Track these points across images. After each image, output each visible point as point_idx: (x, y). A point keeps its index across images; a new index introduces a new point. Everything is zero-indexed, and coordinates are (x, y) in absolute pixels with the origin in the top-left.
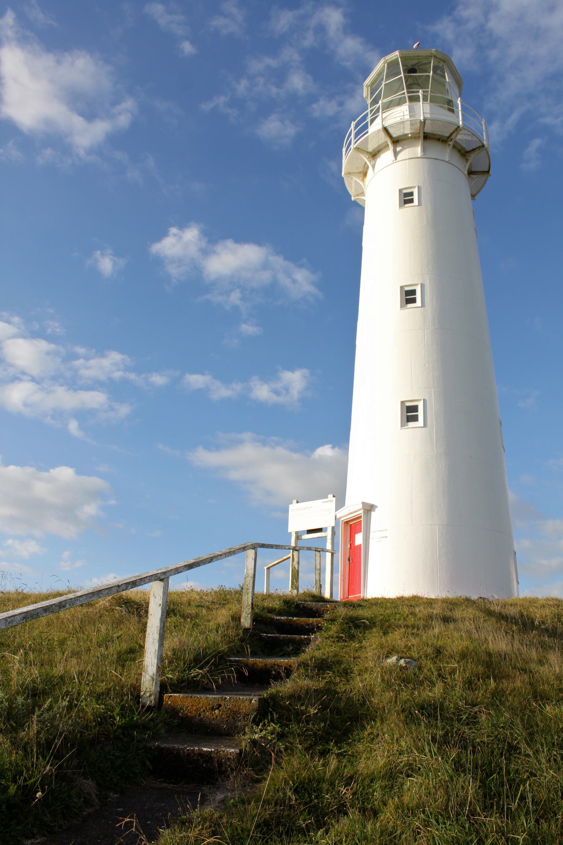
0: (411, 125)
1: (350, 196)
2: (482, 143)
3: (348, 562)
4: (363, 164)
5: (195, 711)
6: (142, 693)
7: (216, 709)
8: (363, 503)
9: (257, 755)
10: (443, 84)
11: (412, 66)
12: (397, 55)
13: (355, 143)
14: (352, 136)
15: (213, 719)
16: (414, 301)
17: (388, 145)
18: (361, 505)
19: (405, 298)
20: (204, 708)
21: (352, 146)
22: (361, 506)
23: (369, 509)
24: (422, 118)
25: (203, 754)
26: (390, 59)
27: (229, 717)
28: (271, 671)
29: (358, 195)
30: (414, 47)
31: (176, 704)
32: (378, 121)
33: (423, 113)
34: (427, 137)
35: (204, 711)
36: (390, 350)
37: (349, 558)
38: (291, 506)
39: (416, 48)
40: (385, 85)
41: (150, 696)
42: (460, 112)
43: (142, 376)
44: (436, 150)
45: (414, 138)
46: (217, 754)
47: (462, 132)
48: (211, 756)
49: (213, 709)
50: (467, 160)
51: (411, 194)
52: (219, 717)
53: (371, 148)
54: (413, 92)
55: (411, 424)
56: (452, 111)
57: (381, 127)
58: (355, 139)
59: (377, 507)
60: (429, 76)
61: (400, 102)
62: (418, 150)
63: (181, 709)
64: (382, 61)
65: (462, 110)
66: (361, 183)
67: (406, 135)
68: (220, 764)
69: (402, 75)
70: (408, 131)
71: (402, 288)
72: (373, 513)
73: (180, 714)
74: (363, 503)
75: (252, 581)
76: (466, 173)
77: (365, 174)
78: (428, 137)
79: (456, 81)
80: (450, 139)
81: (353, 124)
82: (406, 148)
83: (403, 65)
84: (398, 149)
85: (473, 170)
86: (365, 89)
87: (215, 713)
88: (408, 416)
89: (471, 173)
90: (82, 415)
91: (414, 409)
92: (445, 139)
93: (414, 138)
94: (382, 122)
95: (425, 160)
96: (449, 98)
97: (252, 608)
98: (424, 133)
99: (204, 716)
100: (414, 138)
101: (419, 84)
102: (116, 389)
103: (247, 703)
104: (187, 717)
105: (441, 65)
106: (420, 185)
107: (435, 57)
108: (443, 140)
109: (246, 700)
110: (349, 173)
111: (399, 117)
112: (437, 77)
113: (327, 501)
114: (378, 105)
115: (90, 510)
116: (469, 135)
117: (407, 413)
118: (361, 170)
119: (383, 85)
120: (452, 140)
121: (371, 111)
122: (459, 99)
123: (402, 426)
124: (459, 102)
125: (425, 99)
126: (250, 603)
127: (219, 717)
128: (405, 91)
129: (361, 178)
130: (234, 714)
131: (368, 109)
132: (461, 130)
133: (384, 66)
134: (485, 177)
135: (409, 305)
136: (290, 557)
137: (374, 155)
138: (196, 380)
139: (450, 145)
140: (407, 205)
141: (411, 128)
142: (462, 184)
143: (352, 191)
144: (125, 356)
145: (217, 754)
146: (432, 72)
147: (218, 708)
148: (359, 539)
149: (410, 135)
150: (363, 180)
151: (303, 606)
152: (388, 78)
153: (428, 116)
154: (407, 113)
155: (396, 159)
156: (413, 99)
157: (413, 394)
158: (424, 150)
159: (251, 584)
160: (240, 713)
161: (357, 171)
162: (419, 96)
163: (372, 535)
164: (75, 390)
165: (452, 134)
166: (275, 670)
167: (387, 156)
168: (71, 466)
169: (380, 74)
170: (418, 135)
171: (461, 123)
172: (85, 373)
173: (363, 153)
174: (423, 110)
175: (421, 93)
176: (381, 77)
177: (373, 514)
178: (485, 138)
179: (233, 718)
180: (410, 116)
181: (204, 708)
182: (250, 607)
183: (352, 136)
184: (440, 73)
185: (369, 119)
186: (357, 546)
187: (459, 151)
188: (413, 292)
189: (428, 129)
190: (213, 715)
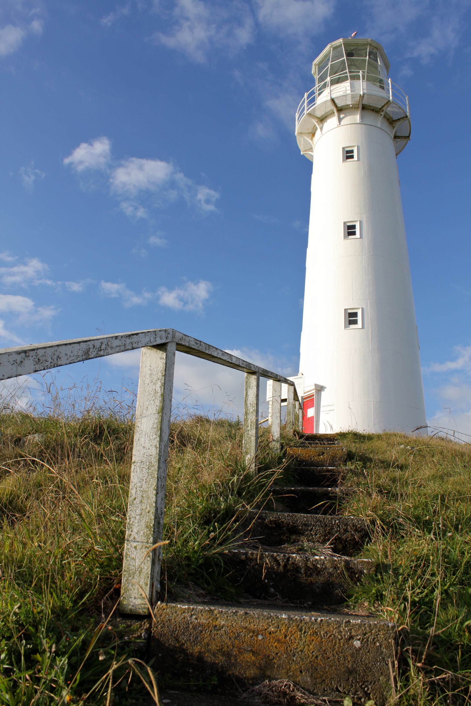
1: (300, 151)
2: (406, 115)
4: (313, 126)
8: (316, 385)
10: (376, 67)
11: (351, 50)
12: (341, 42)
14: (306, 104)
17: (334, 113)
19: (347, 231)
20: (314, 455)
21: (305, 112)
22: (314, 387)
23: (320, 389)
24: (362, 93)
26: (335, 44)
29: (306, 151)
30: (352, 35)
32: (326, 92)
33: (363, 89)
34: (364, 108)
35: (314, 456)
36: (333, 270)
39: (354, 37)
40: (331, 65)
42: (390, 90)
44: (371, 118)
49: (319, 455)
50: (394, 127)
51: (352, 151)
53: (319, 114)
54: (353, 72)
55: (352, 326)
56: (382, 88)
57: (329, 98)
59: (326, 388)
61: (345, 79)
62: (357, 117)
64: (329, 46)
65: (392, 88)
69: (345, 58)
70: (349, 102)
72: (322, 392)
74: (316, 385)
76: (393, 137)
78: (366, 108)
79: (385, 65)
80: (381, 110)
81: (306, 95)
82: (348, 116)
83: (345, 50)
84: (342, 116)
85: (397, 135)
86: (313, 67)
88: (349, 320)
89: (396, 137)
91: (355, 315)
92: (378, 110)
95: (363, 125)
96: (381, 77)
98: (363, 104)
99: (314, 460)
101: (355, 65)
103: (340, 451)
107: (370, 45)
108: (376, 111)
110: (301, 133)
111: (343, 90)
112: (371, 60)
118: (310, 131)
119: (329, 65)
120: (383, 111)
122: (390, 79)
123: (345, 328)
124: (389, 82)
129: (310, 137)
132: (391, 103)
133: (330, 50)
135: (351, 237)
136: (268, 420)
137: (322, 120)
138: (111, 288)
140: (348, 160)
141: (352, 101)
142: (388, 142)
143: (301, 147)
147: (322, 455)
148: (311, 412)
149: (351, 106)
150: (312, 139)
153: (365, 91)
154: (349, 88)
155: (340, 124)
156: (355, 78)
157: (353, 304)
158: (362, 117)
161: (307, 132)
162: (359, 76)
163: (322, 409)
165: (383, 106)
167: (333, 121)
169: (327, 55)
170: (357, 106)
173: (313, 118)
174: (362, 87)
175: (361, 74)
178: (408, 110)
179: (332, 460)
180: (351, 91)
183: (306, 104)
184: (373, 57)
187: (388, 120)
188: (354, 227)
189: (365, 102)
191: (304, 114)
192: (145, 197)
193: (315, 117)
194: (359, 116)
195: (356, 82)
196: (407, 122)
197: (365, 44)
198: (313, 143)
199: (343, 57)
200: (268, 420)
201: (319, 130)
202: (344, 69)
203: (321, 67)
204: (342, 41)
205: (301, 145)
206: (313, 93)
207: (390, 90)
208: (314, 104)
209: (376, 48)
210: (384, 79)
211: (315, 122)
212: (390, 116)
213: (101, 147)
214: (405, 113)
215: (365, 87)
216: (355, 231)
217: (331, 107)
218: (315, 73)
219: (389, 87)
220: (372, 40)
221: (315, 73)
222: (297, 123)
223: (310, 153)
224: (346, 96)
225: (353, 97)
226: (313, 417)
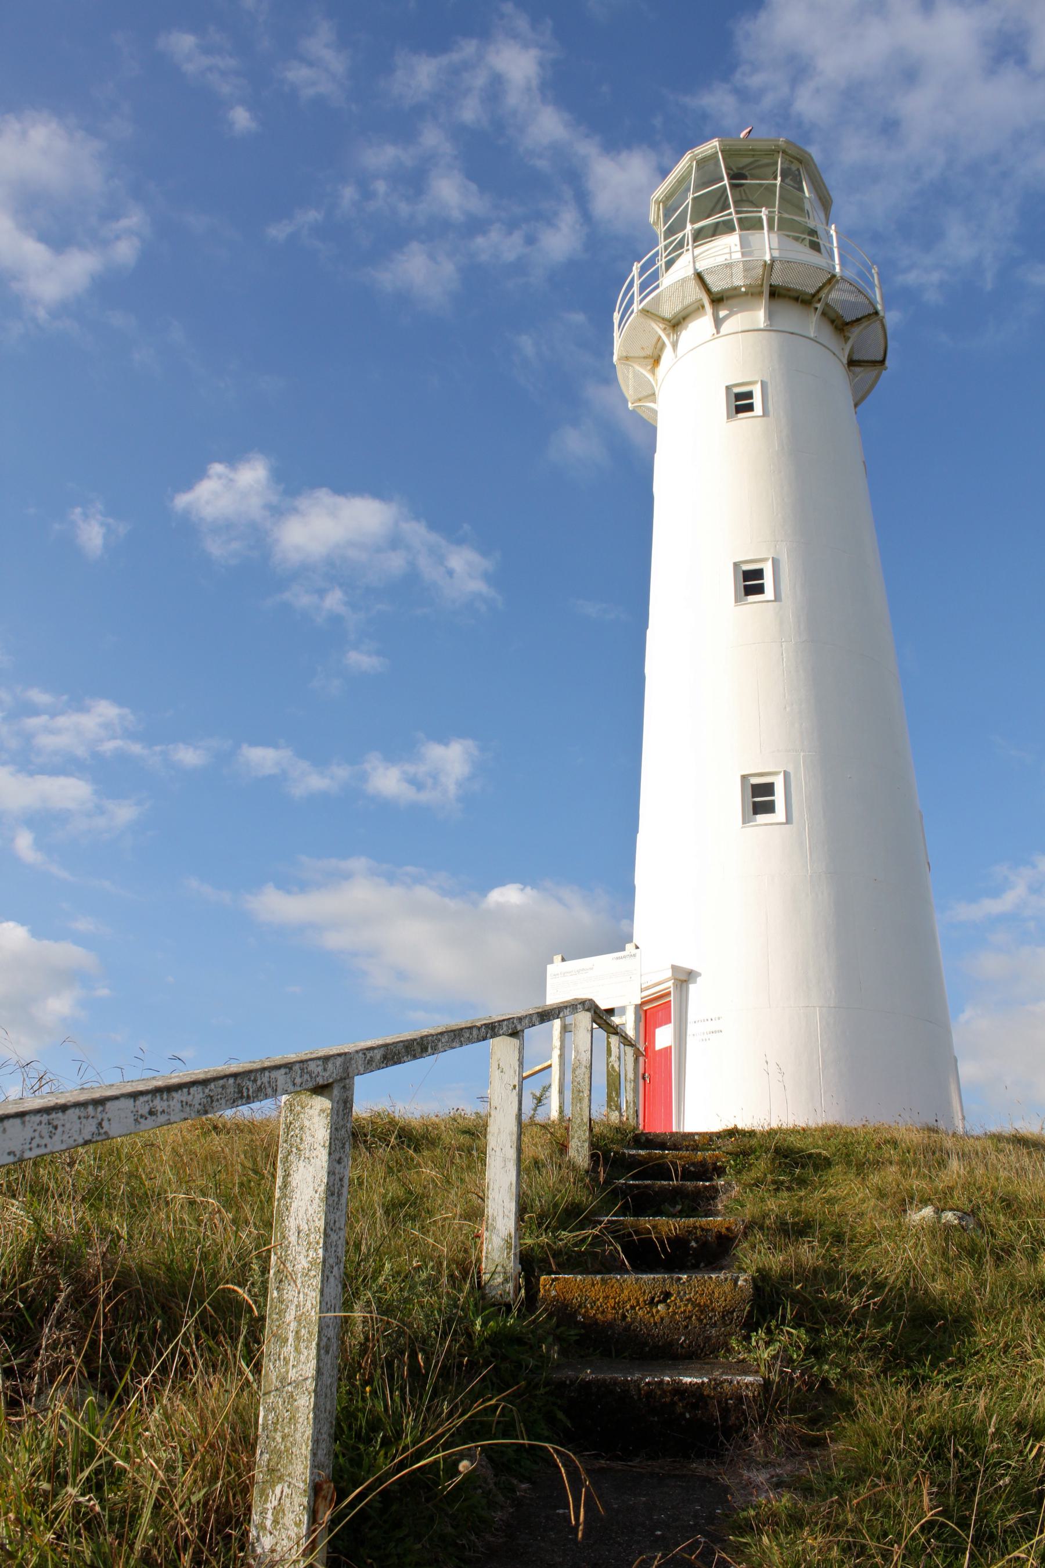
0: (746, 270)
1: (626, 401)
3: (641, 1081)
5: (614, 1308)
6: (486, 1277)
7: (659, 1302)
8: (674, 968)
9: (799, 1387)
12: (715, 147)
13: (641, 301)
14: (636, 288)
15: (655, 1324)
16: (759, 590)
17: (703, 307)
18: (670, 971)
20: (633, 1302)
21: (636, 307)
22: (669, 973)
23: (684, 978)
24: (768, 258)
25: (685, 1391)
26: (702, 152)
27: (690, 1317)
28: (689, 1242)
30: (742, 136)
31: (569, 1296)
33: (770, 249)
34: (776, 293)
35: (633, 1307)
36: (714, 680)
37: (644, 1075)
38: (549, 967)
40: (694, 199)
41: (506, 1281)
42: (836, 251)
43: (158, 748)
44: (792, 317)
45: (752, 293)
46: (715, 1389)
47: (840, 286)
48: (702, 1394)
49: (652, 1303)
51: (749, 395)
52: (667, 1320)
53: (668, 310)
55: (762, 818)
56: (815, 247)
58: (640, 294)
59: (699, 974)
60: (775, 185)
61: (726, 228)
62: (759, 316)
63: (580, 1306)
64: (688, 156)
65: (839, 248)
66: (649, 376)
67: (736, 288)
68: (725, 1411)
69: (726, 182)
71: (736, 565)
73: (580, 1318)
74: (674, 968)
75: (587, 1076)
76: (845, 361)
77: (656, 360)
79: (820, 199)
80: (816, 298)
82: (736, 313)
83: (726, 168)
84: (722, 314)
85: (856, 357)
87: (658, 1311)
88: (754, 803)
89: (852, 363)
90: (43, 821)
93: (752, 293)
94: (694, 262)
95: (772, 333)
97: (591, 1130)
98: (771, 286)
99: (634, 1320)
100: (752, 295)
102: (108, 774)
103: (727, 1288)
104: (596, 1322)
105: (794, 168)
106: (765, 379)
107: (784, 152)
108: (804, 300)
109: (726, 1279)
110: (627, 358)
111: (724, 254)
113: (625, 957)
114: (681, 235)
115: (59, 1005)
116: (852, 292)
117: (753, 797)
118: (649, 352)
120: (820, 300)
121: (666, 248)
122: (833, 227)
123: (744, 822)
124: (833, 232)
125: (771, 228)
126: (586, 1120)
127: (667, 1320)
128: (732, 210)
130: (702, 1312)
131: (685, 228)
132: (838, 281)
133: (691, 166)
134: (875, 373)
135: (752, 598)
136: (550, 1066)
137: (676, 324)
138: (263, 758)
139: (816, 309)
140: (741, 415)
143: (629, 390)
144: (126, 711)
145: (715, 1389)
146: (779, 179)
147: (664, 1301)
148: (664, 1037)
150: (653, 371)
151: (647, 1138)
152: (697, 188)
153: (776, 254)
155: (718, 332)
156: (751, 225)
158: (770, 315)
159: (587, 1081)
160: (713, 1310)
161: (643, 354)
162: (760, 219)
163: (691, 1029)
164: (31, 774)
165: (820, 289)
166: (697, 1240)
167: (701, 326)
168: (22, 922)
169: (683, 180)
170: (759, 289)
171: (838, 269)
172: (47, 741)
173: (654, 321)
174: (767, 245)
175: (764, 213)
176: (684, 186)
177: (692, 987)
180: (743, 254)
181: (633, 1302)
182: (586, 1128)
183: (636, 288)
185: (664, 260)
186: (661, 1050)
187: (832, 322)
188: (758, 574)
189: (777, 279)
190: (653, 1316)
191: (632, 312)
192: (335, 570)
193: (659, 317)
194: (762, 311)
195: (754, 236)
196: (878, 324)
197: (773, 151)
198: (656, 381)
199: (722, 180)
200: (550, 1066)
201: (669, 348)
202: (726, 207)
203: (669, 205)
204: (717, 144)
205: (628, 386)
206: (652, 262)
207: (836, 251)
208: (657, 287)
209: (798, 159)
210: (820, 228)
211: (658, 329)
212: (836, 312)
213: (253, 475)
214: (872, 304)
215: (775, 245)
216: (762, 585)
217: (696, 293)
218: (656, 223)
219: (832, 243)
220: (787, 142)
221: (656, 223)
222: (616, 334)
223: (651, 405)
224: (729, 266)
225: (747, 268)
226: (670, 1047)
